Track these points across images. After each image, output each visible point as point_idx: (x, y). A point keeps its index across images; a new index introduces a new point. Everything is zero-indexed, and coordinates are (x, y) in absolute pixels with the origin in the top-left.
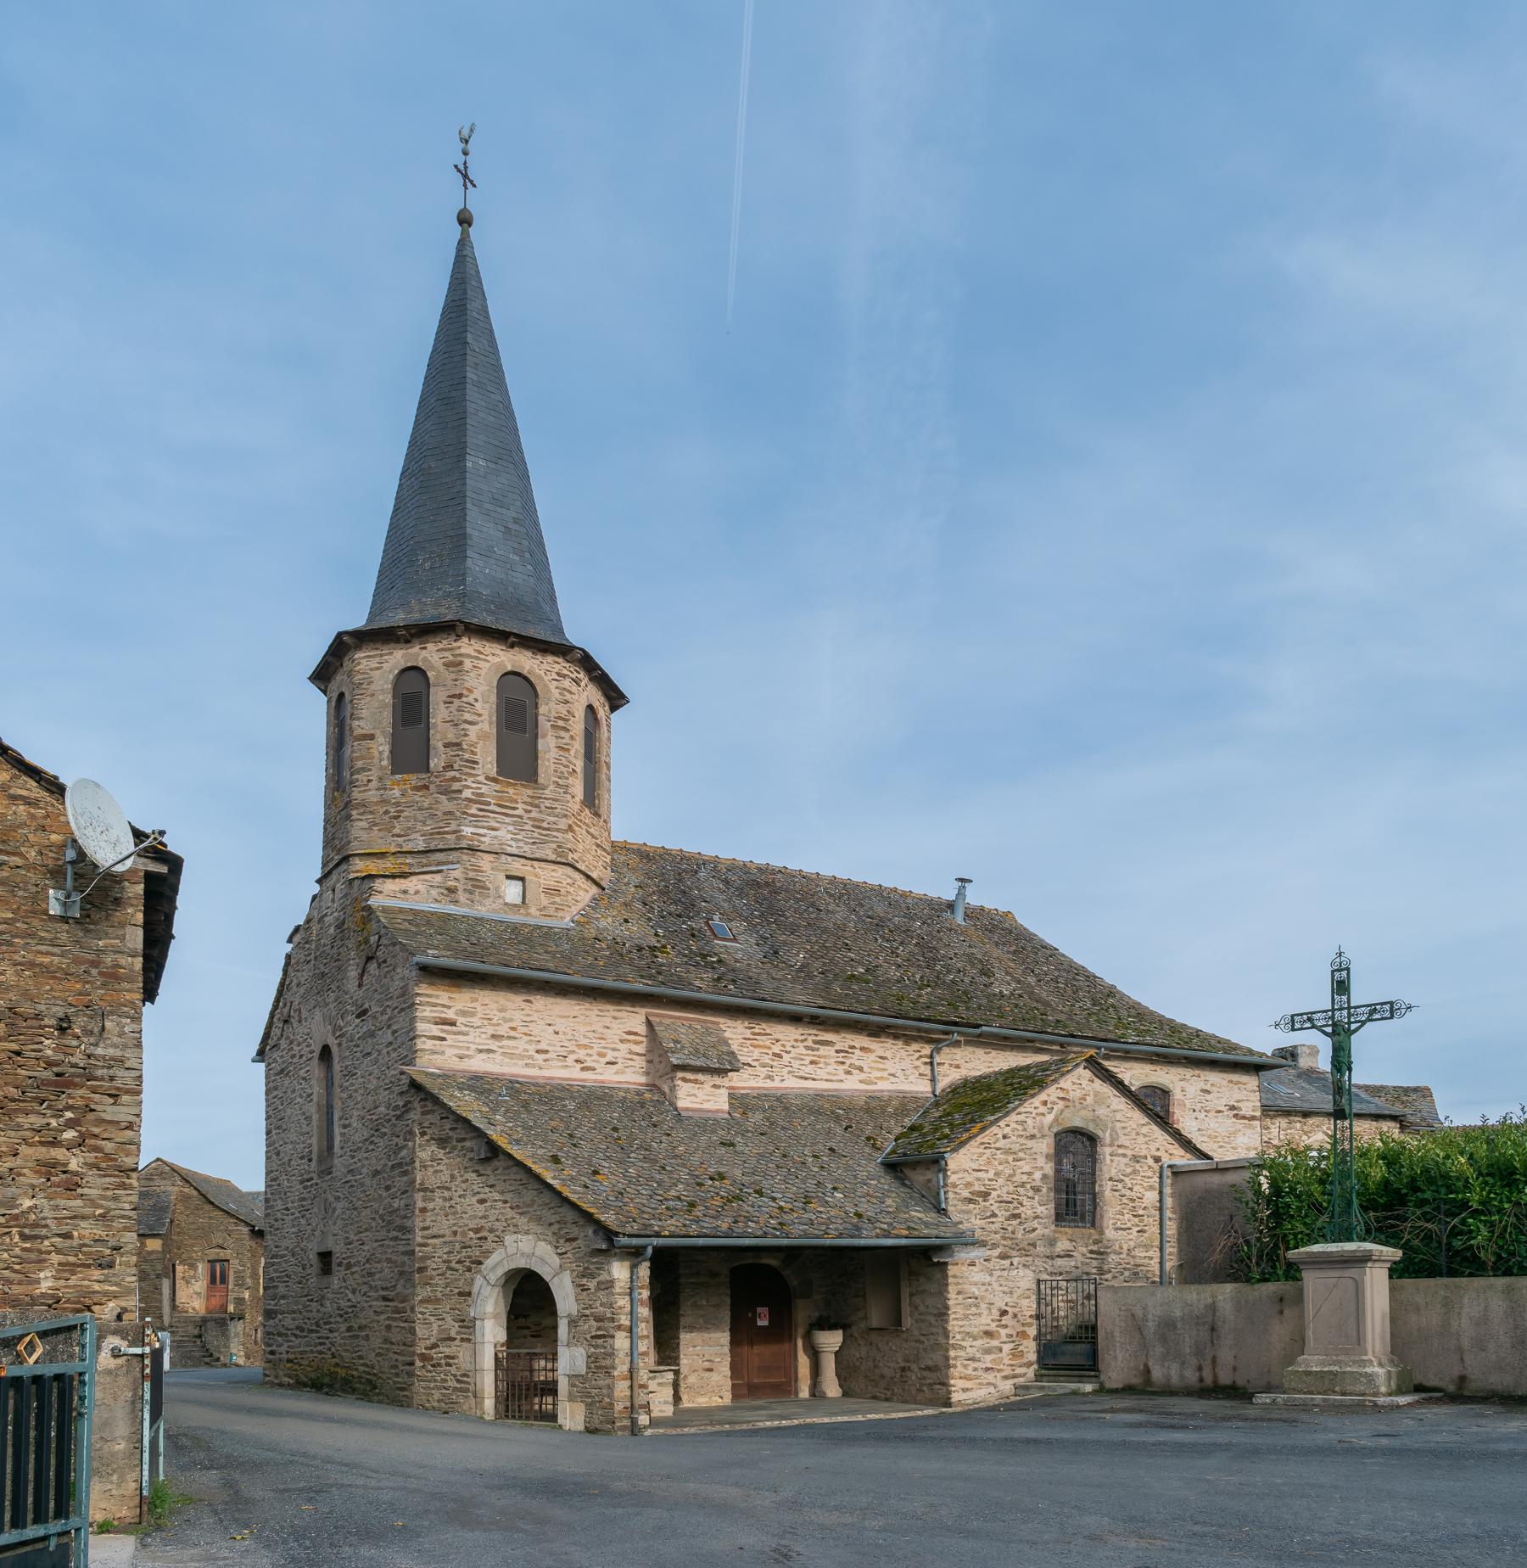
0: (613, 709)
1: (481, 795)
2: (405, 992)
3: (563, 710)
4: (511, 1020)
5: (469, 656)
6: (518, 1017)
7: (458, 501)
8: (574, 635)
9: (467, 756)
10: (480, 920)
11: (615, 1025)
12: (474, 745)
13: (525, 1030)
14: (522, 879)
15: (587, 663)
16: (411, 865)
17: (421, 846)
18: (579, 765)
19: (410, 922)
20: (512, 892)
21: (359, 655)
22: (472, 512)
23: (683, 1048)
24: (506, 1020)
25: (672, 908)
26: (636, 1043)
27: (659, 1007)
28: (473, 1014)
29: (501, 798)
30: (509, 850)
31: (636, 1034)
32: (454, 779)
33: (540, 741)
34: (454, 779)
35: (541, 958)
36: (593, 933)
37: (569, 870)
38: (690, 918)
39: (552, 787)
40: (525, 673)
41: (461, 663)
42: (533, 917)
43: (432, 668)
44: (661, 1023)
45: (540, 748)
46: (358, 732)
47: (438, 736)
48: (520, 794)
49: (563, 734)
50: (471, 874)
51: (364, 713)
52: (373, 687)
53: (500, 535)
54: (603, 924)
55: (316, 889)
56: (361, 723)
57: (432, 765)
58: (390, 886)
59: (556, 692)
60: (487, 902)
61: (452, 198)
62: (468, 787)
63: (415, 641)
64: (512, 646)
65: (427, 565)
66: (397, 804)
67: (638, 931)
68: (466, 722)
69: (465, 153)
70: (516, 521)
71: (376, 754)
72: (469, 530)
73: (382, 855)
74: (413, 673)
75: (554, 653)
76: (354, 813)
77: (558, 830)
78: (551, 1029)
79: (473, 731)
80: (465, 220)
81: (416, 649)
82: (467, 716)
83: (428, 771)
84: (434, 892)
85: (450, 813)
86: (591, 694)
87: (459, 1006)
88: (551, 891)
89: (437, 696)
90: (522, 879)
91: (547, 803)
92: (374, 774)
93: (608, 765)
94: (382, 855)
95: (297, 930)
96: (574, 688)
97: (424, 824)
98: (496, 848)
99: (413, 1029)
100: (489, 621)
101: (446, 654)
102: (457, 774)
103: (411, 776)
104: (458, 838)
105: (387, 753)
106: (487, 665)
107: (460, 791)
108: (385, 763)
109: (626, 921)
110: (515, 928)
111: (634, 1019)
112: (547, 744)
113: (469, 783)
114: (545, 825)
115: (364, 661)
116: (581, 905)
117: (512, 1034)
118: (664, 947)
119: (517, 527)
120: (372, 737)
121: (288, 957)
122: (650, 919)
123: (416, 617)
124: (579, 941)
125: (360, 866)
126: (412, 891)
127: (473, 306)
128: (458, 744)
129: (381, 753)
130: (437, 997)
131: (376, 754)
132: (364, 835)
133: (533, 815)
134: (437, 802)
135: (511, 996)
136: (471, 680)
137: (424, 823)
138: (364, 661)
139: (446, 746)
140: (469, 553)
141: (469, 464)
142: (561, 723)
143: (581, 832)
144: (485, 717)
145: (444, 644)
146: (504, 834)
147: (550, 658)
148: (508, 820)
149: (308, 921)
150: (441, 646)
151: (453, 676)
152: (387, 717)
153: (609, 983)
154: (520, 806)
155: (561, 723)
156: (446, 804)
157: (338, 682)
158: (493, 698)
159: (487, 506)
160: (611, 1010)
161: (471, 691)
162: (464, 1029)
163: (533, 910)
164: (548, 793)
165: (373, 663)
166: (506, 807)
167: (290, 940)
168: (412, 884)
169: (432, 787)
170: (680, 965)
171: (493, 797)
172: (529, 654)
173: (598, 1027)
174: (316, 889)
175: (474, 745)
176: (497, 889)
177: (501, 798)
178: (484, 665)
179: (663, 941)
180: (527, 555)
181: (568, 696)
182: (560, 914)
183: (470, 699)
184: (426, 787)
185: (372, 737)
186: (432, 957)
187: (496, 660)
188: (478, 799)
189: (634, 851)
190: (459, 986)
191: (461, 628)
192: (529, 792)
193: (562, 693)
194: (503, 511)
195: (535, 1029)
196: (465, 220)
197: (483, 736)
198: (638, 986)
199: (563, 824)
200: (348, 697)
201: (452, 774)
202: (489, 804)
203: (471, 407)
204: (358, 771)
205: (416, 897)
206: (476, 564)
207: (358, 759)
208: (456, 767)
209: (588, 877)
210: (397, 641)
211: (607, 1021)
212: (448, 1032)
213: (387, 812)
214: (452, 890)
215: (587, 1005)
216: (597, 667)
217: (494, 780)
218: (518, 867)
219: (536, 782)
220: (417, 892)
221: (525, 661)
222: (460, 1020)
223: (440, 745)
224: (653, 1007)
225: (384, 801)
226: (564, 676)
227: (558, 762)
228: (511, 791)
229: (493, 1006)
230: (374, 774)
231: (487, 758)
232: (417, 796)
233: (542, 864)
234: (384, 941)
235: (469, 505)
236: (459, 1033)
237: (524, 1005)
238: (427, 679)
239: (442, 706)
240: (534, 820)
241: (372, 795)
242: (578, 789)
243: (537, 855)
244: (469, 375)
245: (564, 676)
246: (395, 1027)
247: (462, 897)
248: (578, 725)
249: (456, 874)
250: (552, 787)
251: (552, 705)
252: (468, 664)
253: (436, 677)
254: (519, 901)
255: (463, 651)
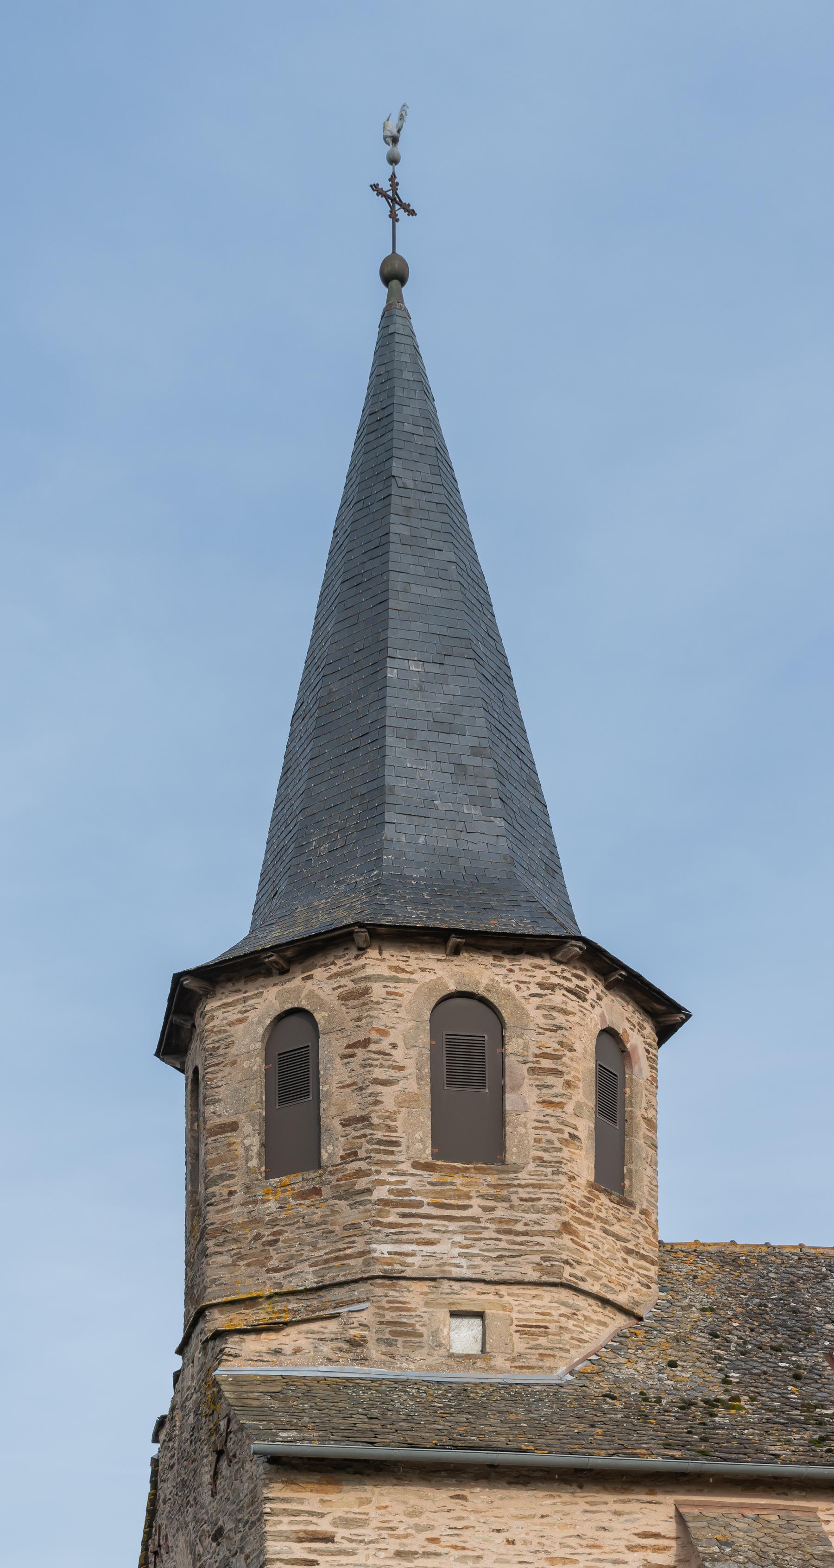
0: (664, 1033)
1: (407, 1192)
2: (255, 1500)
3: (551, 1042)
4: (430, 1528)
5: (379, 978)
6: (441, 1524)
7: (373, 738)
8: (592, 924)
9: (379, 1135)
10: (402, 1384)
11: (617, 1524)
12: (391, 1116)
13: (455, 1541)
14: (480, 1315)
15: (598, 961)
16: (296, 1311)
17: (311, 1281)
18: (585, 1127)
19: (273, 1395)
20: (464, 1337)
21: (212, 1005)
22: (396, 749)
23: (736, 1552)
24: (419, 1528)
25: (766, 1338)
26: (657, 1549)
27: (700, 1492)
28: (363, 1523)
29: (441, 1194)
30: (456, 1272)
31: (656, 1536)
32: (360, 1173)
33: (509, 1097)
34: (360, 1173)
35: (491, 1427)
36: (606, 1387)
37: (564, 1294)
38: (796, 1351)
39: (531, 1167)
40: (481, 991)
41: (366, 991)
42: (502, 1370)
43: (322, 1005)
44: (696, 1518)
45: (508, 1107)
46: (214, 1121)
47: (333, 1111)
48: (474, 1184)
49: (550, 1080)
50: (389, 1316)
51: (223, 1093)
52: (234, 1050)
53: (447, 778)
54: (627, 1371)
55: (177, 1362)
56: (218, 1108)
57: (324, 1156)
58: (252, 1345)
59: (537, 1017)
60: (418, 1355)
61: (370, 236)
62: (383, 1183)
63: (296, 968)
64: (456, 951)
65: (324, 849)
66: (274, 1222)
67: (695, 1378)
68: (377, 1082)
69: (393, 161)
70: (476, 751)
71: (241, 1151)
72: (389, 780)
73: (252, 1301)
74: (294, 1019)
75: (533, 953)
76: (210, 1243)
77: (543, 1233)
78: (500, 1538)
79: (389, 1095)
80: (394, 274)
81: (297, 982)
82: (379, 1073)
83: (318, 1165)
84: (326, 1349)
85: (354, 1226)
86: (619, 1012)
87: (339, 1512)
88: (526, 1329)
89: (330, 1049)
90: (480, 1315)
91: (523, 1193)
92: (238, 1183)
93: (652, 1124)
94: (252, 1301)
95: (161, 1423)
96: (573, 1004)
97: (314, 1246)
98: (434, 1272)
99: (262, 1551)
100: (416, 917)
101: (342, 981)
102: (363, 1165)
103: (293, 1178)
104: (367, 1264)
105: (255, 1149)
106: (413, 988)
107: (369, 1191)
108: (254, 1163)
109: (672, 1364)
110: (462, 1390)
111: (657, 1513)
112: (523, 1102)
113: (384, 1176)
114: (519, 1227)
115: (219, 1014)
116: (588, 1348)
117: (432, 1548)
118: (736, 1399)
119: (477, 761)
120: (233, 1127)
121: (155, 1462)
122: (718, 1358)
123: (298, 932)
124: (578, 1402)
125: (219, 1320)
126: (288, 1350)
127: (405, 416)
128: (364, 1119)
129: (247, 1149)
130: (301, 1501)
131: (241, 1151)
132: (226, 1276)
133: (498, 1214)
134: (334, 1212)
135: (429, 1492)
136: (384, 1016)
137: (314, 1246)
138: (219, 1014)
139: (345, 1123)
140: (389, 816)
141: (392, 674)
142: (546, 1063)
143: (591, 1233)
144: (411, 1070)
145: (340, 965)
146: (449, 1249)
147: (526, 962)
148: (452, 1226)
149: (173, 1409)
150: (335, 969)
151: (355, 1013)
152: (255, 1095)
153: (600, 1460)
154: (475, 1202)
155: (546, 1063)
156: (347, 1213)
157: (195, 1057)
158: (425, 1039)
159: (423, 736)
160: (610, 1501)
161: (383, 1032)
162: (347, 1545)
163: (499, 1361)
164: (523, 1176)
165: (233, 1014)
166: (448, 1207)
167: (155, 1439)
168: (288, 1339)
169: (326, 1191)
170: (751, 1425)
171: (427, 1194)
172: (488, 960)
173: (588, 1529)
174: (177, 1362)
175: (391, 1116)
176: (435, 1334)
177: (441, 1194)
178: (406, 988)
179: (735, 1391)
180: (496, 803)
181: (560, 1019)
182: (548, 1362)
183: (384, 1045)
184: (317, 1191)
185: (233, 1127)
186: (289, 1441)
187: (429, 977)
188: (402, 1200)
189: (710, 1256)
190: (338, 1483)
191: (362, 936)
192: (492, 1179)
193: (550, 1017)
194: (454, 739)
195: (471, 1539)
196: (394, 274)
197: (407, 1101)
198: (656, 1462)
199: (552, 1222)
200: (201, 1072)
201: (356, 1165)
202: (420, 1204)
203: (396, 581)
204: (214, 1182)
205: (296, 1359)
206: (401, 833)
207: (214, 1162)
208: (362, 1153)
209: (605, 1302)
210: (268, 974)
211: (604, 1519)
212: (321, 1553)
213: (258, 1237)
214: (355, 1343)
215: (566, 1497)
216: (616, 964)
217: (428, 1167)
218: (470, 1297)
219: (503, 1162)
220: (297, 1351)
221: (481, 973)
222: (341, 1533)
223: (336, 1123)
224: (689, 1492)
225: (255, 1221)
226: (553, 987)
227: (542, 1125)
228: (458, 1180)
229: (399, 1508)
230: (238, 1183)
231: (415, 1134)
232: (303, 1207)
233: (515, 1289)
234: (234, 1426)
235: (390, 740)
236: (340, 1552)
237: (451, 1504)
238: (315, 1024)
239: (338, 1063)
240: (501, 1221)
241: (237, 1214)
242: (583, 1164)
243: (506, 1276)
244: (393, 528)
245: (553, 987)
246: (247, 1551)
247: (374, 1351)
248: (582, 1065)
249: (363, 1317)
250: (531, 1167)
251: (531, 1037)
252: (378, 991)
253: (328, 1020)
254: (476, 1349)
255: (369, 971)
